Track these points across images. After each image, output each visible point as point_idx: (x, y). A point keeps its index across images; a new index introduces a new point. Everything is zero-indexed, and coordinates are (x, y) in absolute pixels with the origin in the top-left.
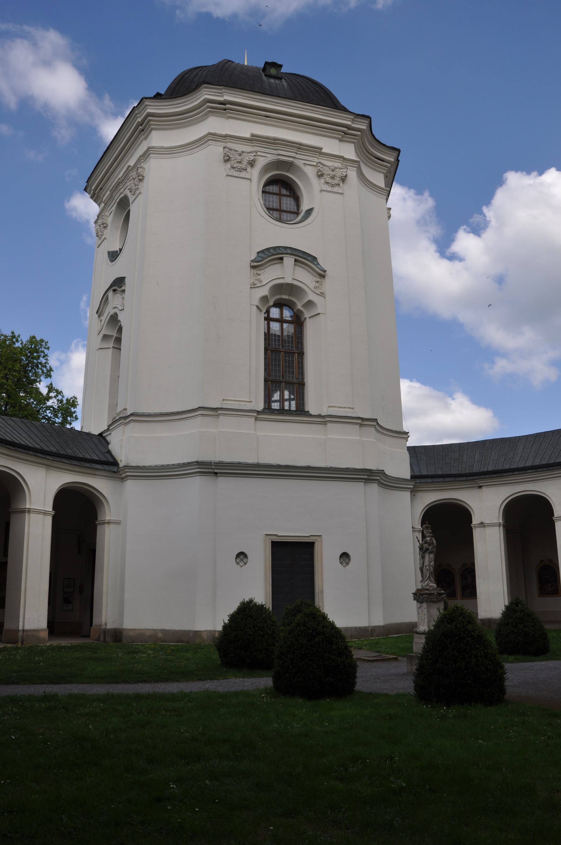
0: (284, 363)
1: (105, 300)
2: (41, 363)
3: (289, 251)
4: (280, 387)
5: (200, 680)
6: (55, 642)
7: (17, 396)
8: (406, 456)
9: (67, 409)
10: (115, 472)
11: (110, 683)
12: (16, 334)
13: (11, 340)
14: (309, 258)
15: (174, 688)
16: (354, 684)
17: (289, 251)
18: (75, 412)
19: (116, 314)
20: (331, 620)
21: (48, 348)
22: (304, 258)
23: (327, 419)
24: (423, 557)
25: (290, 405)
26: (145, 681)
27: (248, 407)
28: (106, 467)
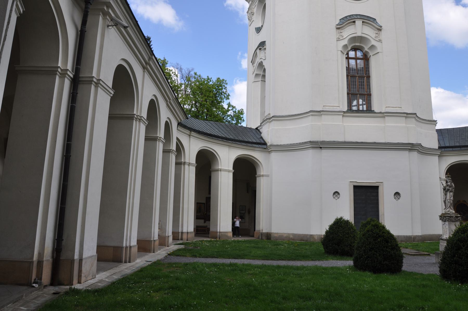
0: (359, 84)
1: (255, 54)
2: (223, 92)
3: (359, 17)
4: (356, 97)
5: (313, 260)
6: (236, 239)
7: (212, 110)
8: (436, 135)
9: (238, 116)
10: (265, 148)
11: (264, 260)
12: (210, 78)
13: (208, 81)
14: (371, 20)
15: (298, 263)
16: (401, 266)
17: (359, 17)
18: (243, 117)
19: (262, 62)
20: (387, 229)
21: (227, 84)
22: (368, 20)
23: (385, 114)
24: (446, 195)
25: (363, 107)
26: (283, 260)
27: (338, 109)
28: (260, 146)
